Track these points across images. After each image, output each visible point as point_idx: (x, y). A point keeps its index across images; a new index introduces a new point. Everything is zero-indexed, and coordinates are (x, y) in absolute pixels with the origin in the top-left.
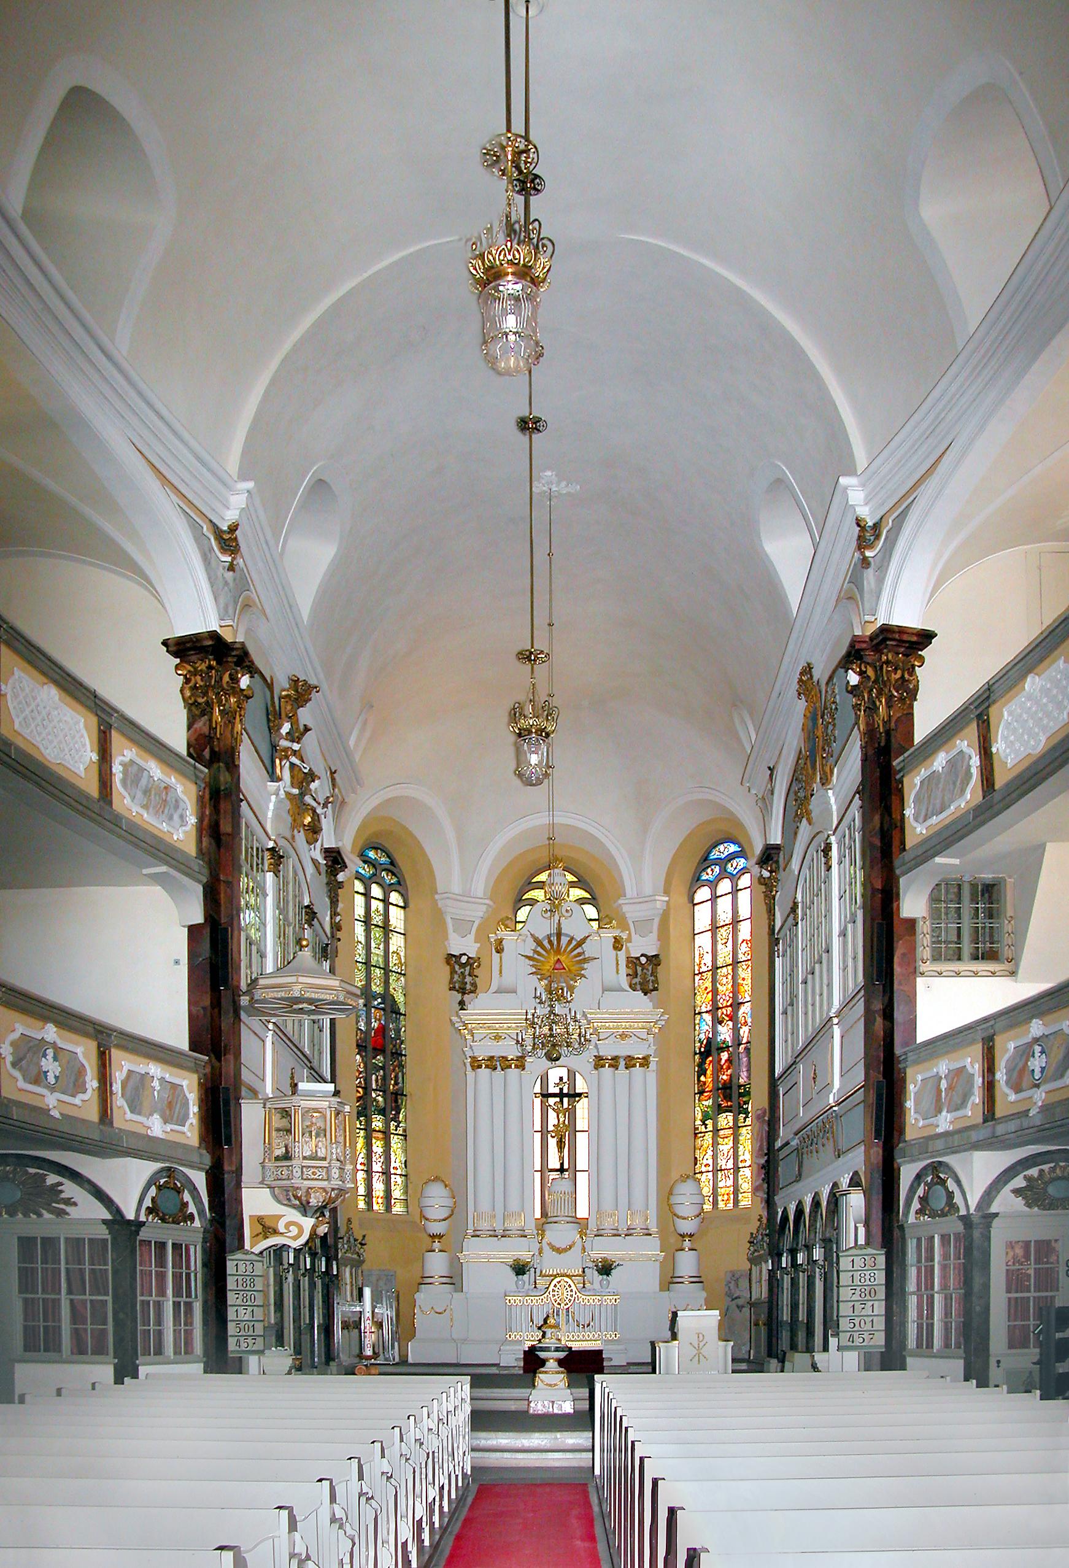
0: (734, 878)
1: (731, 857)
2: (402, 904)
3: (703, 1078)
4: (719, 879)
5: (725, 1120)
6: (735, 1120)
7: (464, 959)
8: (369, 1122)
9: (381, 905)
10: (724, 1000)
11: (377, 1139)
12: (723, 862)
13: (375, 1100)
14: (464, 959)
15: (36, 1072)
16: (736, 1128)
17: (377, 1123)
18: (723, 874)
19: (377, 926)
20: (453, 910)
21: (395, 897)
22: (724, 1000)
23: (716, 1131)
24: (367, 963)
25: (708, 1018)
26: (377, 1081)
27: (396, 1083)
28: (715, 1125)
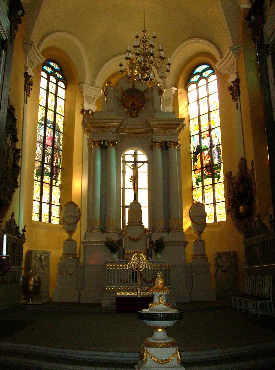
0: (206, 78)
1: (204, 71)
2: (64, 88)
3: (196, 163)
4: (199, 80)
5: (208, 181)
6: (213, 181)
7: (90, 112)
8: (42, 178)
9: (54, 86)
10: (205, 127)
11: (46, 187)
12: (200, 74)
13: (46, 168)
14: (90, 112)
15: (155, 275)
16: (213, 184)
17: (47, 179)
18: (201, 77)
19: (51, 93)
20: (86, 92)
21: (61, 84)
22: (205, 127)
23: (203, 187)
24: (46, 108)
25: (197, 137)
26: (47, 160)
27: (57, 162)
28: (203, 183)
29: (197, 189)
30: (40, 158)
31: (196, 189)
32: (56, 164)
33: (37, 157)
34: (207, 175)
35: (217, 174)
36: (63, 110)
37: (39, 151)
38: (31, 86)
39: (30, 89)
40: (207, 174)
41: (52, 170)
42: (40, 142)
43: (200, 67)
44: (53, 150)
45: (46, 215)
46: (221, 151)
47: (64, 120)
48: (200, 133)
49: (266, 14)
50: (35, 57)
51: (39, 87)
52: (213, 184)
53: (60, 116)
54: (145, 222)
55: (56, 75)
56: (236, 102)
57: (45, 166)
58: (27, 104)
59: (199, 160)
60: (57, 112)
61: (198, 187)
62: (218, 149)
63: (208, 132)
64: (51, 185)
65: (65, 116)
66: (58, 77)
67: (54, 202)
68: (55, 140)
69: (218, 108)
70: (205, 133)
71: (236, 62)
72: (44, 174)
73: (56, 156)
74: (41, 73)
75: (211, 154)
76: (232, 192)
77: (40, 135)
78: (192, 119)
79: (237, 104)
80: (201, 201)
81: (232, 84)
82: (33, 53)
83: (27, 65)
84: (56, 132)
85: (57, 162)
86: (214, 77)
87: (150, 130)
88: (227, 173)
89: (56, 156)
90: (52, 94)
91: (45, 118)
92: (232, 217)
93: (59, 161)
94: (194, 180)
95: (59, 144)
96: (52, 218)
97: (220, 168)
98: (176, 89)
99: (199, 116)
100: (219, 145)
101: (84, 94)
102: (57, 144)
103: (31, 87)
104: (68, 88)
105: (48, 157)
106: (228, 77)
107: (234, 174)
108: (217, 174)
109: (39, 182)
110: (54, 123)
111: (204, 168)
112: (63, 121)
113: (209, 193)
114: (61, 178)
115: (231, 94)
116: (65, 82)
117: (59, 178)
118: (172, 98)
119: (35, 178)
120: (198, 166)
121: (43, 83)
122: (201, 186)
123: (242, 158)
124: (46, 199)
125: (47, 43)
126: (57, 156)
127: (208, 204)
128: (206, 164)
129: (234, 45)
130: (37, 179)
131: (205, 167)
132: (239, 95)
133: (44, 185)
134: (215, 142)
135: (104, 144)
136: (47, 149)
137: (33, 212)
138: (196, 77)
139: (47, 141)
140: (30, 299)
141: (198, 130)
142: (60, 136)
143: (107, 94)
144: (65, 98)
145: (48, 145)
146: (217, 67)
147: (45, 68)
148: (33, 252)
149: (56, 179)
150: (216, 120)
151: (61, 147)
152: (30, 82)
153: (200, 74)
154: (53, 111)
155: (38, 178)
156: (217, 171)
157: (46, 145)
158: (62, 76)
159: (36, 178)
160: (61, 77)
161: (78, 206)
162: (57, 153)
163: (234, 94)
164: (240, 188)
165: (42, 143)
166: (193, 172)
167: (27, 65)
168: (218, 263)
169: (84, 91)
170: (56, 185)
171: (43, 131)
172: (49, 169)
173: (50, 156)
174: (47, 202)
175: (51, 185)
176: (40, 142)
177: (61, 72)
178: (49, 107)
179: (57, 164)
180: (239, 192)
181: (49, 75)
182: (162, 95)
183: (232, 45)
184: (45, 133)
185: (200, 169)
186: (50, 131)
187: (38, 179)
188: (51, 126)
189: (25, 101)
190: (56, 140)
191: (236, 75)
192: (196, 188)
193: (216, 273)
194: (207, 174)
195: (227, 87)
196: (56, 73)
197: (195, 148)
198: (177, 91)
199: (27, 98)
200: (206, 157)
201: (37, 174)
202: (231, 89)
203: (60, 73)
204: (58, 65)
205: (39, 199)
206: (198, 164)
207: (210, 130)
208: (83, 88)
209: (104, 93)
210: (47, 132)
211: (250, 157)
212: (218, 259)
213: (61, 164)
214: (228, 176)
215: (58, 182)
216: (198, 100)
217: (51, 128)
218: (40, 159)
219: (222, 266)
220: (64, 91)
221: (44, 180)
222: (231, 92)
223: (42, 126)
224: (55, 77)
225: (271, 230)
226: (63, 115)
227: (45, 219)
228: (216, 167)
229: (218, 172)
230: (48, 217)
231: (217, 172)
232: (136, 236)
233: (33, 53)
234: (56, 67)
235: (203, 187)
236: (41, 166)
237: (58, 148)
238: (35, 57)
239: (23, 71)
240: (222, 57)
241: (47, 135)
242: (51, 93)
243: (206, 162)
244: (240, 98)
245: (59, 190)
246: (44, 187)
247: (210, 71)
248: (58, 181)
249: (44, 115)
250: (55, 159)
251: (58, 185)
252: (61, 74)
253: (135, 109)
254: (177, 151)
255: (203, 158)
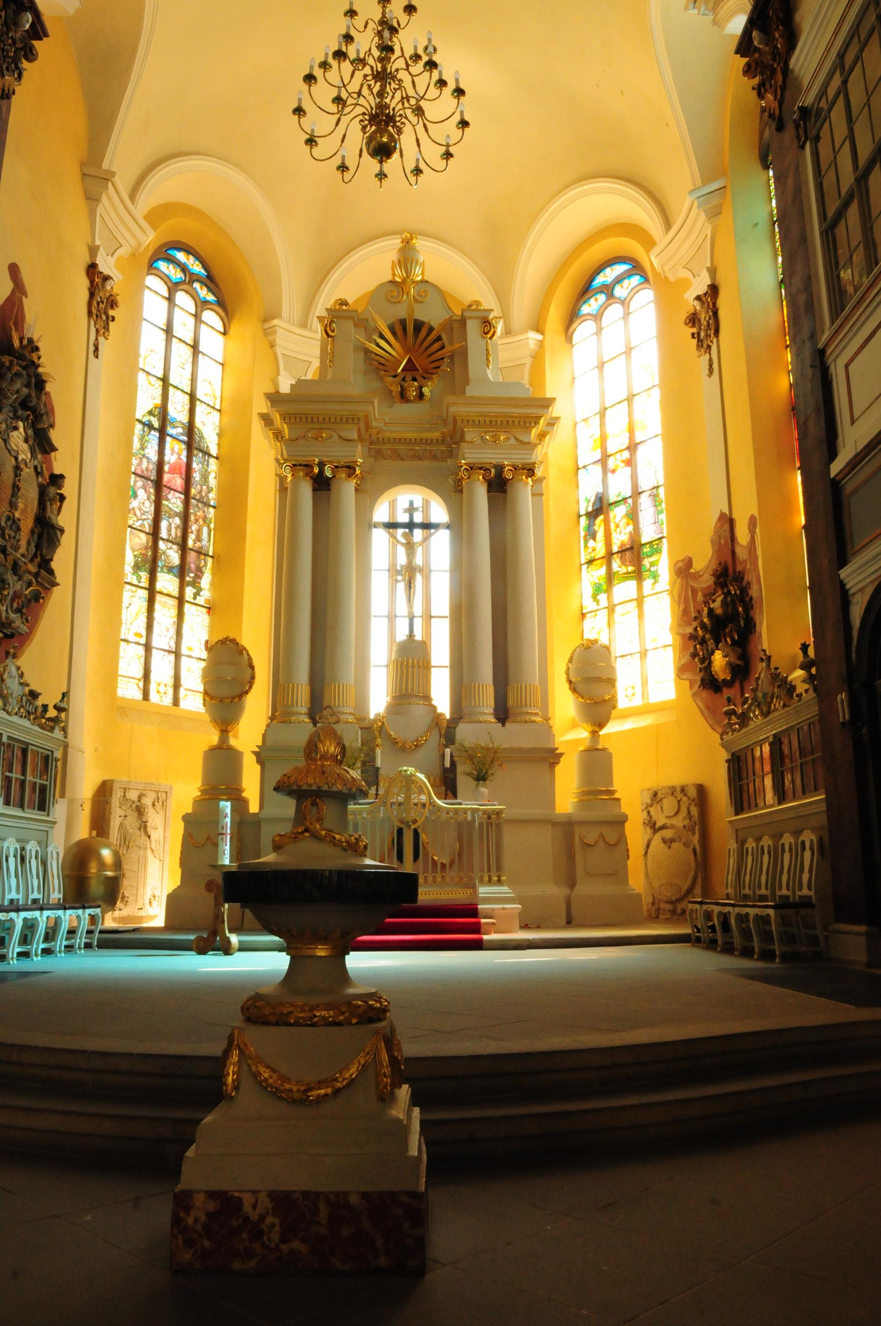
0: (624, 303)
1: (619, 280)
3: (591, 543)
5: (625, 590)
6: (640, 588)
10: (617, 442)
11: (164, 605)
13: (164, 553)
17: (167, 582)
26: (169, 530)
27: (198, 539)
28: (609, 599)
29: (596, 615)
30: (145, 522)
31: (593, 614)
32: (195, 543)
33: (138, 520)
34: (624, 574)
35: (652, 569)
36: (218, 394)
37: (143, 503)
38: (112, 307)
39: (111, 319)
40: (624, 570)
41: (183, 558)
42: (147, 479)
43: (608, 271)
44: (187, 503)
45: (166, 686)
46: (663, 506)
47: (221, 421)
48: (604, 460)
49: (798, 17)
50: (121, 219)
51: (137, 318)
52: (640, 600)
53: (208, 408)
54: (442, 700)
55: (195, 290)
56: (707, 355)
57: (162, 545)
58: (97, 357)
59: (600, 535)
60: (198, 396)
61: (597, 608)
62: (654, 497)
63: (626, 455)
64: (181, 600)
65: (223, 409)
66: (202, 296)
67: (190, 649)
68: (194, 475)
69: (657, 382)
70: (618, 455)
71: (709, 236)
72: (159, 570)
73: (197, 521)
74: (143, 280)
75: (633, 516)
76: (693, 615)
77: (148, 458)
78: (584, 420)
79: (711, 360)
80: (604, 640)
81: (697, 304)
82: (115, 209)
83: (98, 242)
84: (195, 452)
85: (198, 539)
86: (647, 295)
87: (453, 439)
88: (678, 562)
89: (197, 521)
90: (184, 345)
91: (163, 412)
92: (691, 686)
93: (205, 535)
94: (587, 590)
95: (204, 487)
96: (182, 692)
97: (658, 551)
98: (540, 337)
99: (603, 413)
100: (658, 487)
101: (279, 351)
102: (199, 487)
103: (111, 313)
104: (234, 328)
105: (171, 520)
106: (684, 284)
107: (698, 565)
108: (652, 569)
109: (143, 590)
110: (190, 429)
111: (615, 556)
112: (217, 423)
113: (626, 616)
114: (213, 584)
115: (693, 334)
116: (222, 314)
117: (206, 581)
118: (528, 361)
119: (131, 578)
120: (597, 550)
121: (153, 306)
122: (606, 605)
123: (722, 516)
124: (163, 637)
125: (162, 188)
126: (200, 520)
127: (626, 656)
128: (619, 543)
129: (706, 182)
130: (135, 582)
131: (618, 553)
132: (717, 332)
133: (159, 598)
134: (645, 484)
135: (321, 471)
136: (168, 500)
137: (120, 673)
138: (596, 300)
139: (166, 477)
140: (357, 962)
141: (599, 451)
142: (208, 466)
143: (333, 331)
144: (224, 360)
145: (171, 489)
146: (653, 260)
147: (162, 265)
148: (116, 786)
149: (195, 583)
150: (650, 417)
151: (212, 495)
152: (108, 295)
153: (607, 290)
154: (187, 393)
155: (139, 578)
156: (651, 559)
157: (165, 486)
158: (215, 296)
159: (135, 577)
160: (211, 298)
161: (247, 652)
162: (200, 513)
163: (702, 334)
164: (714, 601)
165: (152, 481)
166: (584, 567)
167: (98, 242)
168: (651, 817)
169: (278, 341)
170: (196, 602)
171: (156, 448)
172: (174, 557)
173: (177, 521)
174: (167, 648)
175: (181, 600)
176: (147, 479)
177: (210, 281)
178: (172, 380)
179: (198, 544)
180: (711, 611)
181: (173, 287)
182: (491, 338)
183: (699, 182)
184: (161, 452)
185: (603, 558)
186: (176, 449)
187: (140, 582)
188: (181, 434)
189: (92, 348)
190: (196, 476)
191: (708, 275)
192: (591, 612)
193: (648, 846)
194: (624, 570)
195: (684, 316)
196: (197, 285)
197: (589, 501)
198: (541, 344)
199: (97, 339)
200: (621, 525)
201: (137, 567)
202: (693, 319)
203: (207, 287)
204: (200, 262)
205: (142, 637)
206: (599, 548)
207: (632, 447)
208: (275, 332)
209: (326, 333)
210: (167, 451)
211: (745, 509)
212: (651, 806)
213: (212, 543)
214: (683, 569)
215: (201, 593)
216: (601, 366)
217: (180, 441)
218: (147, 526)
219: (663, 827)
220: (221, 338)
221: (159, 586)
222: (695, 330)
223: (153, 432)
224: (194, 295)
225: (806, 691)
226: (218, 407)
227: (161, 696)
228: (646, 550)
229: (652, 564)
230: (171, 691)
231: (650, 563)
232: (409, 736)
233: (115, 209)
234: (197, 268)
235: (611, 609)
236: (150, 544)
237: (202, 497)
238: (121, 219)
239: (84, 259)
240: (668, 224)
241: (166, 458)
242: (180, 340)
243: (620, 538)
244: (718, 341)
245: (207, 616)
246: (157, 606)
247: (636, 280)
248: (201, 590)
249: (158, 401)
250: (194, 528)
251: (202, 603)
252: (210, 289)
253: (414, 379)
254: (532, 495)
255: (613, 526)
